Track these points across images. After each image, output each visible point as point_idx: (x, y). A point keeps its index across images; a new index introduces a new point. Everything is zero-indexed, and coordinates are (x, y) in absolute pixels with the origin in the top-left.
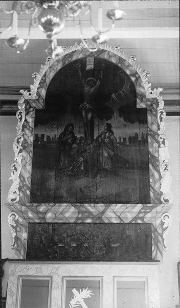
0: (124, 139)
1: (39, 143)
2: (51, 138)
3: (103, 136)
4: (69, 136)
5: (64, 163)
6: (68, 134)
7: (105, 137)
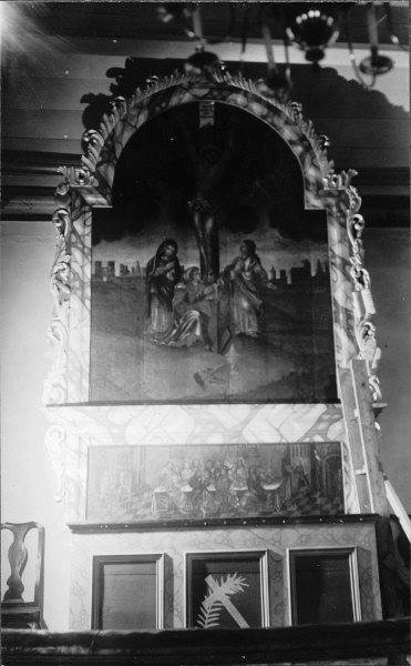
0: (283, 273)
1: (105, 279)
2: (130, 269)
3: (238, 267)
4: (168, 266)
5: (160, 321)
6: (165, 263)
7: (243, 269)
